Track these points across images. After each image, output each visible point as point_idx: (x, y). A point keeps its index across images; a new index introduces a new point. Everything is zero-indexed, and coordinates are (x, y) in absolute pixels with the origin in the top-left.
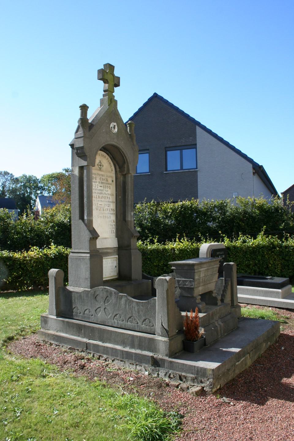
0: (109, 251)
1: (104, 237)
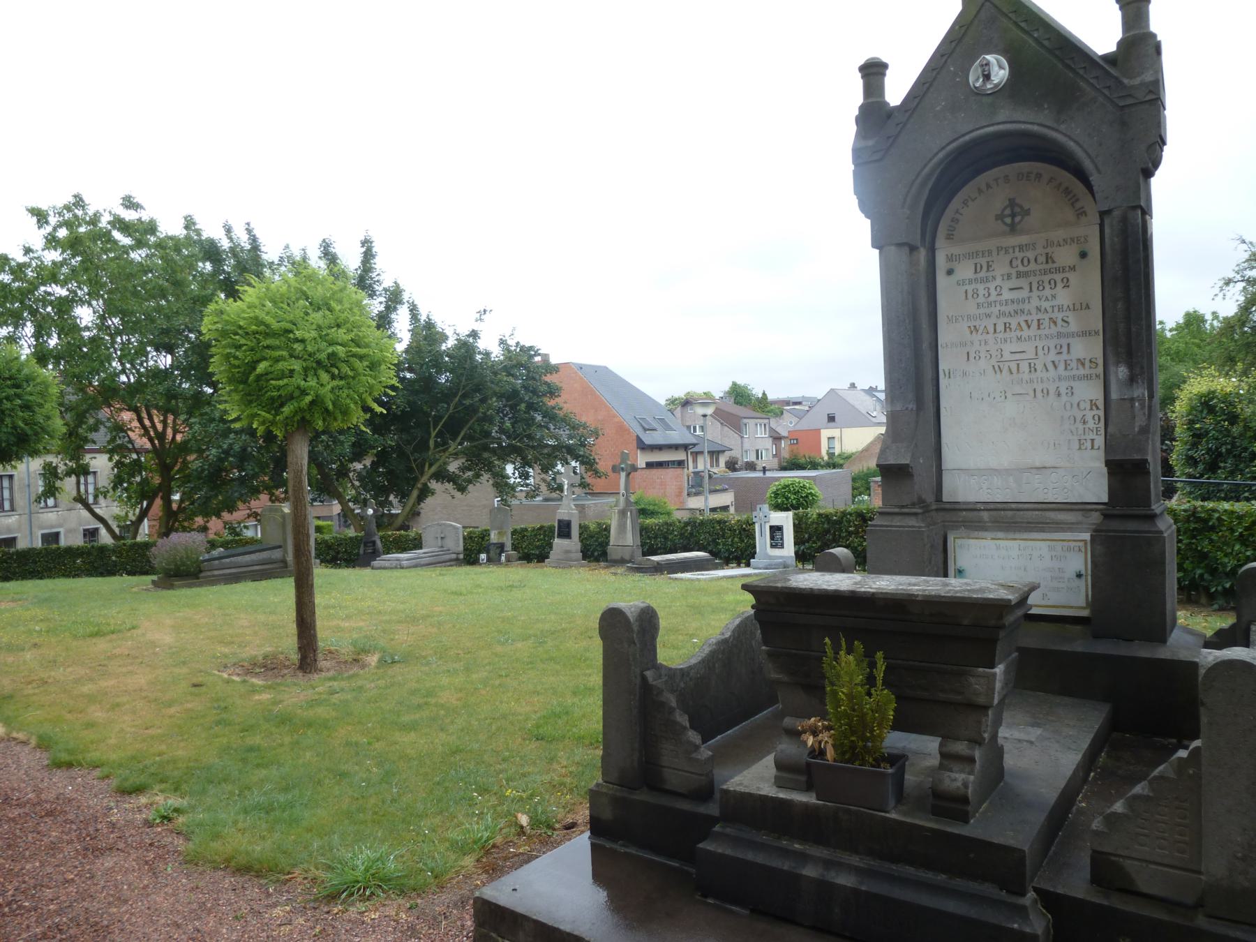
0: (979, 506)
1: (1038, 464)
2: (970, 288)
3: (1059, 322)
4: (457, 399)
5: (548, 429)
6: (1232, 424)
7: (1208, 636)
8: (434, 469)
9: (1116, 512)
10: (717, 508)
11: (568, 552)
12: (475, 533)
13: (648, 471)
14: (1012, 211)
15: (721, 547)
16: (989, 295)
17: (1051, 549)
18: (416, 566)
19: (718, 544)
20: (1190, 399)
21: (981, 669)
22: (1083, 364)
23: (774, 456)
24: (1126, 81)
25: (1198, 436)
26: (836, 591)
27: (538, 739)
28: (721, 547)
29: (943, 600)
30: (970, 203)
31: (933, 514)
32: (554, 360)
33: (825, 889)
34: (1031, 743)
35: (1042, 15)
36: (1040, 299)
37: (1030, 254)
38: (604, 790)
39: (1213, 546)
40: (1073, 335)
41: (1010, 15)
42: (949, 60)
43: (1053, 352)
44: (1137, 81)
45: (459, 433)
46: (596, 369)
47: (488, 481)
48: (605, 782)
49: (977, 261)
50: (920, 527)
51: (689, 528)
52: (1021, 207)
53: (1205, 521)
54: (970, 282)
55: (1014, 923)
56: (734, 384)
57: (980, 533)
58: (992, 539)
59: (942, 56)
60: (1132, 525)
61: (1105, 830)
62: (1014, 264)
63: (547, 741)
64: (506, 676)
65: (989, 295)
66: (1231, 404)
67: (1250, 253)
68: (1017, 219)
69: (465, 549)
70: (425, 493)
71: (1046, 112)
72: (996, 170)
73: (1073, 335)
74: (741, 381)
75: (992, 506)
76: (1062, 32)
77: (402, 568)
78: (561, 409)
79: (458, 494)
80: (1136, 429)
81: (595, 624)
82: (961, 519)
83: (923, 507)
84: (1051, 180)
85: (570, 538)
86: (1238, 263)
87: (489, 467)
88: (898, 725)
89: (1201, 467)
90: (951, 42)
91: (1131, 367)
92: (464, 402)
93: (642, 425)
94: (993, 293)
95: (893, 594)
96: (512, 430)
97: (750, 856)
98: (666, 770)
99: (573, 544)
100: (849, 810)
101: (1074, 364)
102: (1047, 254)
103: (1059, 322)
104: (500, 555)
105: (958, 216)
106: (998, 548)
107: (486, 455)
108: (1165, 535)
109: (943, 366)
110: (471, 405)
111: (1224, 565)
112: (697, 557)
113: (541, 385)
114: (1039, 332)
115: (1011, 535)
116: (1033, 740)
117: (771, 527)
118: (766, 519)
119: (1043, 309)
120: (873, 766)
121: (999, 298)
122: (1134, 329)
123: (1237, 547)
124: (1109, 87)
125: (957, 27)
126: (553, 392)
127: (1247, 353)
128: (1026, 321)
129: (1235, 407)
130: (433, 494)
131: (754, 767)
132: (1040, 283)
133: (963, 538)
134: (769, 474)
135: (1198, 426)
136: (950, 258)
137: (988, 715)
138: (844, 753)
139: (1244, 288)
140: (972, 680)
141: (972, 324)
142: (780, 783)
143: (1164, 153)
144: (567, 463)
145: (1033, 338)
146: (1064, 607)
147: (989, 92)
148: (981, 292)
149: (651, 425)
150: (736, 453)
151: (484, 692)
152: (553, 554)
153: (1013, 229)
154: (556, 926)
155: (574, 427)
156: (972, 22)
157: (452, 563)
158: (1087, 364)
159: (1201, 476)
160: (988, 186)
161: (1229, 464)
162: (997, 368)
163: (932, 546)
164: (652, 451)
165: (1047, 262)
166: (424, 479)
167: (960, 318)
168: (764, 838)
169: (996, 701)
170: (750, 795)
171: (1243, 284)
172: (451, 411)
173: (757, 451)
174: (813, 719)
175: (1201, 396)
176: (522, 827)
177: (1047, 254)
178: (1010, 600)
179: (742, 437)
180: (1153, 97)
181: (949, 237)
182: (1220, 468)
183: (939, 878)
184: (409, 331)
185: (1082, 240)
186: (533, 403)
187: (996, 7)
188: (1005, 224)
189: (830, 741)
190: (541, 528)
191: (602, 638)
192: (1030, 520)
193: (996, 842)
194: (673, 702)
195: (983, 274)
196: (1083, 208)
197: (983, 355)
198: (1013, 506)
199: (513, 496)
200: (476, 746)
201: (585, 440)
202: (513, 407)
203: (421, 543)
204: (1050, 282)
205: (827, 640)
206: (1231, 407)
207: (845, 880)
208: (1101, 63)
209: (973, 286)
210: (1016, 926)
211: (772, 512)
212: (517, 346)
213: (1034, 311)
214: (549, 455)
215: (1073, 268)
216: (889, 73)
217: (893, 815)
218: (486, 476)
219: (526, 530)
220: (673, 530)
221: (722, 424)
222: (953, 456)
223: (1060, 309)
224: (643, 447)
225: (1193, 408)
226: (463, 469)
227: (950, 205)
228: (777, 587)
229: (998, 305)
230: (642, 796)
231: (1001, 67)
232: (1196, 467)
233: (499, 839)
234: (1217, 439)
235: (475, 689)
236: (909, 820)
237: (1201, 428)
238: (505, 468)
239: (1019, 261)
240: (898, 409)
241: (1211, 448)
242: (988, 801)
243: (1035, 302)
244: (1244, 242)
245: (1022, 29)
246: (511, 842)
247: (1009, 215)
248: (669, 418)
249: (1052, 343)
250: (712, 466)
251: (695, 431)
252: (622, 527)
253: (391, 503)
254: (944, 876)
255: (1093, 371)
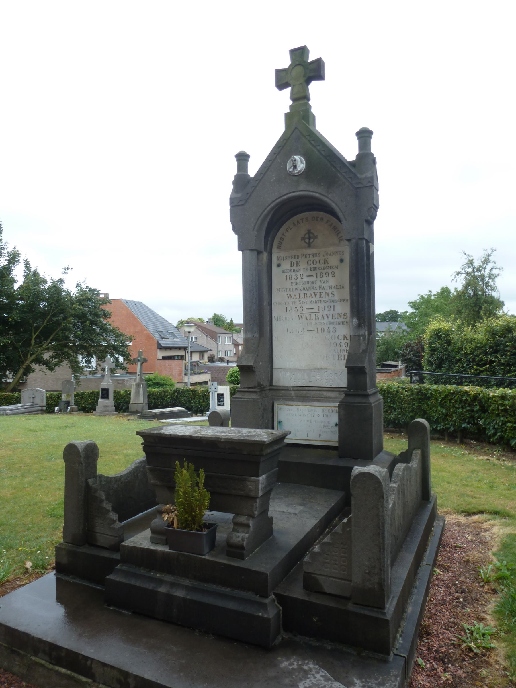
0: (290, 388)
1: (319, 367)
2: (288, 274)
3: (330, 294)
4: (49, 317)
5: (103, 336)
6: (448, 345)
7: (397, 455)
8: (33, 357)
9: (351, 393)
10: (197, 383)
11: (107, 406)
12: (53, 395)
13: (163, 361)
14: (309, 236)
15: (193, 405)
16: (297, 279)
17: (323, 411)
18: (15, 414)
19: (191, 403)
20: (430, 332)
21: (252, 478)
22: (341, 316)
23: (235, 354)
24: (359, 175)
25: (433, 351)
26: (182, 436)
27: (51, 517)
28: (193, 405)
29: (234, 441)
30: (289, 230)
31: (267, 392)
32: (110, 298)
33: (169, 597)
34: (296, 514)
35: (322, 139)
36: (321, 282)
37: (317, 259)
38: (64, 547)
39: (429, 407)
40: (336, 301)
41: (306, 137)
42: (278, 156)
43: (327, 309)
44: (363, 176)
45: (49, 337)
46: (136, 303)
47: (67, 364)
48: (65, 542)
49: (292, 260)
50: (257, 399)
51: (176, 394)
52: (313, 234)
53: (426, 394)
54: (288, 271)
55: (260, 613)
56: (215, 315)
57: (290, 402)
58: (296, 405)
59: (274, 154)
60: (358, 400)
61: (310, 561)
62: (309, 263)
63: (57, 518)
64: (45, 480)
65: (297, 279)
66: (448, 335)
67: (468, 260)
68: (312, 240)
69: (47, 404)
70: (28, 370)
71: (322, 187)
72: (302, 214)
73: (336, 301)
74: (219, 313)
75: (296, 388)
76: (331, 148)
77: (7, 415)
78: (110, 325)
79: (49, 372)
80: (361, 351)
81: (61, 453)
82: (281, 395)
83: (260, 388)
84: (328, 221)
85: (108, 399)
86: (463, 264)
87: (68, 356)
88: (211, 508)
89: (434, 366)
90: (279, 147)
91: (359, 319)
92: (53, 319)
93: (160, 336)
94: (299, 278)
95: (210, 438)
96: (81, 336)
97: (133, 582)
98: (98, 534)
99: (110, 402)
100: (185, 554)
101: (336, 316)
102: (325, 259)
103: (330, 294)
104: (67, 408)
105: (283, 237)
106: (298, 410)
107: (66, 350)
108: (373, 405)
109: (274, 314)
110: (57, 321)
111: (433, 417)
112: (178, 410)
113: (100, 311)
114: (321, 299)
115: (304, 404)
116: (297, 513)
117: (218, 394)
118: (215, 390)
119: (322, 287)
120: (198, 530)
121: (302, 280)
122: (360, 300)
123: (439, 408)
124: (351, 178)
125: (282, 140)
126: (106, 315)
127: (466, 309)
128: (314, 293)
129: (450, 337)
130: (33, 371)
131: (144, 532)
132: (321, 274)
133: (282, 405)
134: (230, 364)
135: (433, 345)
136: (279, 258)
137: (256, 502)
138: (182, 524)
139: (465, 277)
140: (248, 483)
141: (289, 293)
142: (153, 541)
143: (378, 213)
144: (113, 356)
145: (317, 302)
146: (329, 441)
147: (296, 175)
148: (294, 277)
149: (165, 335)
150: (214, 352)
151: (28, 489)
152: (98, 408)
153: (309, 245)
154: (16, 628)
155: (117, 336)
156: (288, 139)
157: (38, 412)
158: (343, 316)
159: (434, 371)
160: (298, 222)
161: (446, 365)
162: (300, 316)
163: (264, 409)
164: (166, 350)
165: (325, 263)
166: (27, 363)
167: (283, 290)
168: (142, 571)
169: (260, 494)
170: (135, 548)
171: (465, 275)
172: (44, 324)
173: (226, 351)
174: (168, 506)
175: (436, 330)
176: (27, 569)
177: (325, 259)
178: (265, 442)
179: (217, 344)
180: (370, 184)
181: (279, 247)
182: (442, 367)
183: (227, 590)
184: (23, 276)
185: (341, 253)
186: (94, 321)
187: (300, 132)
188: (306, 242)
189: (176, 518)
190: (93, 392)
191: (65, 461)
192: (314, 396)
193: (254, 570)
194: (103, 497)
195: (294, 267)
196: (342, 237)
197: (293, 309)
198: (306, 388)
199: (82, 373)
200: (13, 521)
201: (124, 342)
202: (82, 323)
203: (20, 400)
204: (326, 274)
205: (177, 462)
206: (448, 337)
207: (179, 593)
208: (348, 165)
209: (290, 273)
210: (260, 614)
211: (219, 386)
212: (87, 288)
213: (318, 288)
214: (103, 351)
215: (337, 267)
216: (250, 160)
217: (206, 557)
218: (65, 362)
219: (83, 394)
220: (167, 395)
221: (206, 336)
222: (278, 361)
223: (330, 287)
224: (161, 348)
225: (431, 337)
226: (53, 357)
227: (280, 231)
228: (153, 433)
229: (301, 284)
230: (85, 550)
231: (302, 163)
232: (432, 366)
233: (11, 577)
234: (441, 352)
235: (24, 488)
236: (213, 559)
237: (434, 347)
238: (77, 357)
239: (312, 262)
240: (249, 336)
241: (439, 357)
242: (259, 548)
243: (319, 283)
244: (465, 254)
245: (312, 144)
246: (19, 578)
247: (308, 238)
248: (176, 332)
249: (326, 305)
250: (200, 359)
251: (192, 339)
252: (137, 393)
253: (7, 376)
254: (229, 589)
255: (345, 320)
